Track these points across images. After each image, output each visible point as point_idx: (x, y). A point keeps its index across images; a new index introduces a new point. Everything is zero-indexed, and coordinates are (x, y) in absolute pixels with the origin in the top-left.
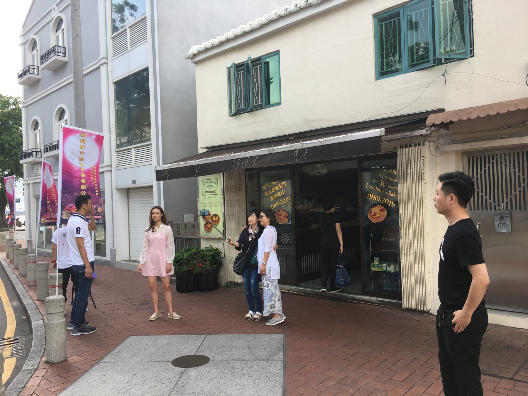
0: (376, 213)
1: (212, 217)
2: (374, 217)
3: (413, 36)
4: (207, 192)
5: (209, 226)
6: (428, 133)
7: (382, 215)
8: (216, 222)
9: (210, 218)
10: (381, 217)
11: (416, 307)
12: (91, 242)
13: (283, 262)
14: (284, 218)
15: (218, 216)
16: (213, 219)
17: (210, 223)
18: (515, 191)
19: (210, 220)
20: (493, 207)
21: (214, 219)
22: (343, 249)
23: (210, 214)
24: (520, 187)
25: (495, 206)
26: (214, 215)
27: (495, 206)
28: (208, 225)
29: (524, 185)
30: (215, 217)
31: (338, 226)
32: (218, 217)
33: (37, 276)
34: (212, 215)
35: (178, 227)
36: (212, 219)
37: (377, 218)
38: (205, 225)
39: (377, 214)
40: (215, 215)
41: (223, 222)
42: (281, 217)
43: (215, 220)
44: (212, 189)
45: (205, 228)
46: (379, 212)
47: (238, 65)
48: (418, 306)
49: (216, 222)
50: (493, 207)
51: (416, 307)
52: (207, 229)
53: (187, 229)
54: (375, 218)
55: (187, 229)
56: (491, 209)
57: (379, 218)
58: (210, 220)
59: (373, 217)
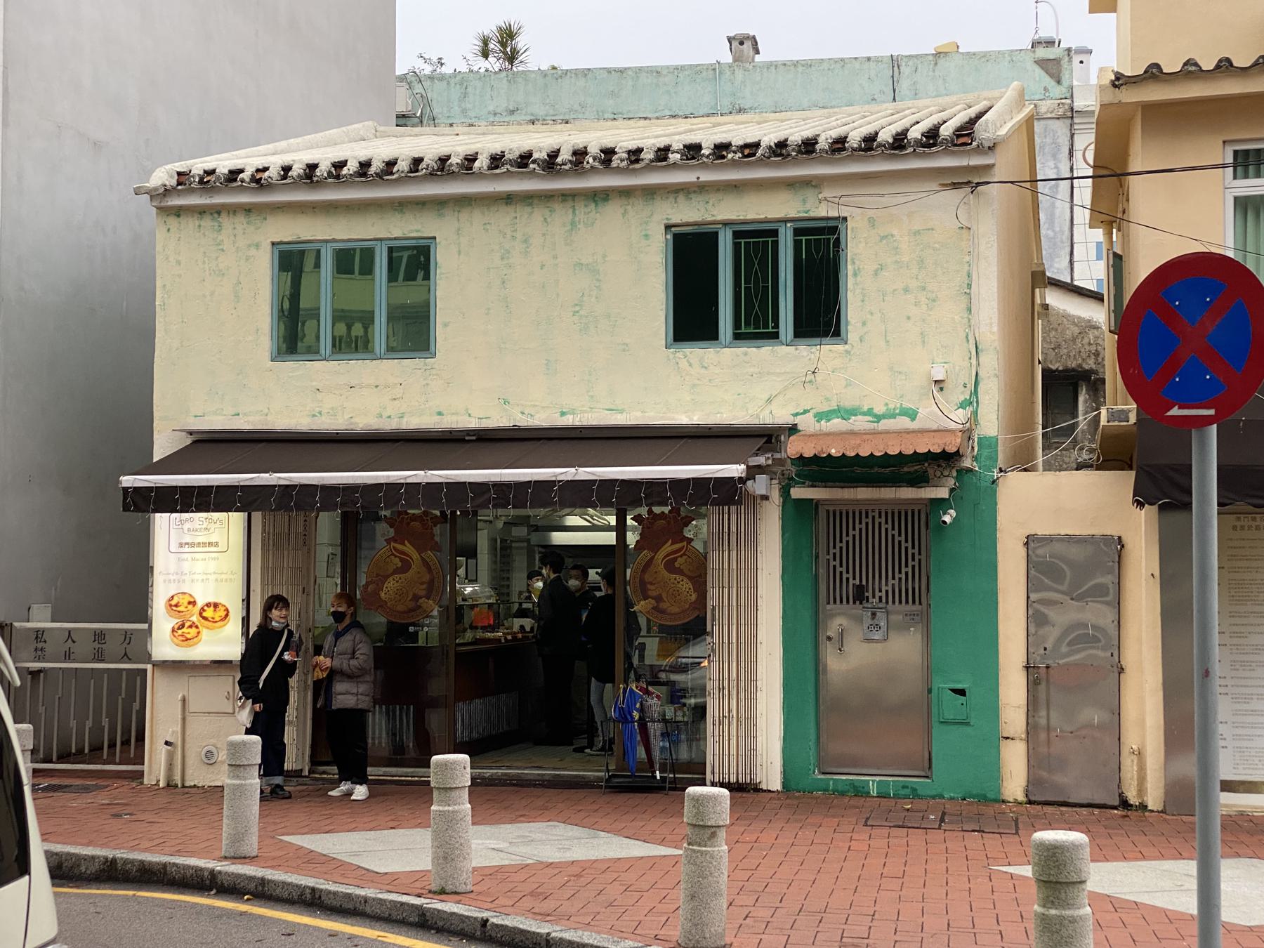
4: (188, 544)
5: (189, 633)
6: (770, 462)
11: (737, 779)
13: (374, 733)
16: (205, 614)
18: (900, 572)
20: (883, 514)
23: (193, 603)
24: (854, 536)
25: (880, 517)
27: (880, 517)
29: (913, 563)
31: (132, 755)
33: (436, 621)
34: (200, 604)
35: (37, 638)
36: (201, 614)
41: (243, 619)
43: (213, 618)
44: (213, 539)
45: (175, 639)
48: (740, 776)
49: (216, 622)
50: (883, 514)
51: (737, 779)
52: (183, 641)
53: (74, 642)
55: (74, 642)
56: (886, 513)
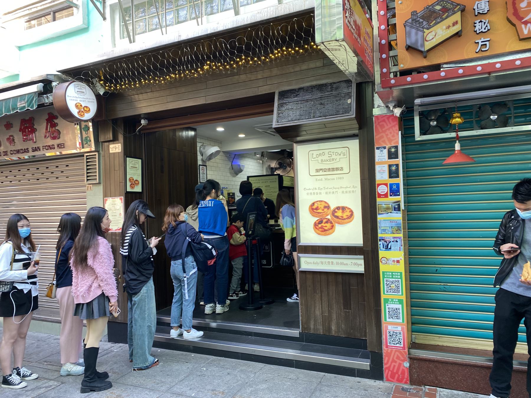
0: (319, 208)
1: (135, 181)
2: (315, 211)
3: (413, 128)
5: (326, 226)
7: (324, 212)
8: (345, 219)
9: (134, 181)
10: (323, 213)
12: (109, 215)
14: (323, 210)
15: (347, 207)
17: (133, 184)
19: (134, 183)
21: (136, 182)
22: (293, 270)
26: (136, 180)
28: (323, 224)
30: (341, 211)
32: (349, 210)
34: (135, 180)
37: (319, 213)
38: (130, 185)
39: (319, 209)
40: (137, 180)
42: (320, 211)
43: (342, 217)
46: (322, 208)
47: (252, 137)
49: (345, 219)
54: (316, 212)
57: (321, 214)
58: (134, 183)
59: (314, 211)
